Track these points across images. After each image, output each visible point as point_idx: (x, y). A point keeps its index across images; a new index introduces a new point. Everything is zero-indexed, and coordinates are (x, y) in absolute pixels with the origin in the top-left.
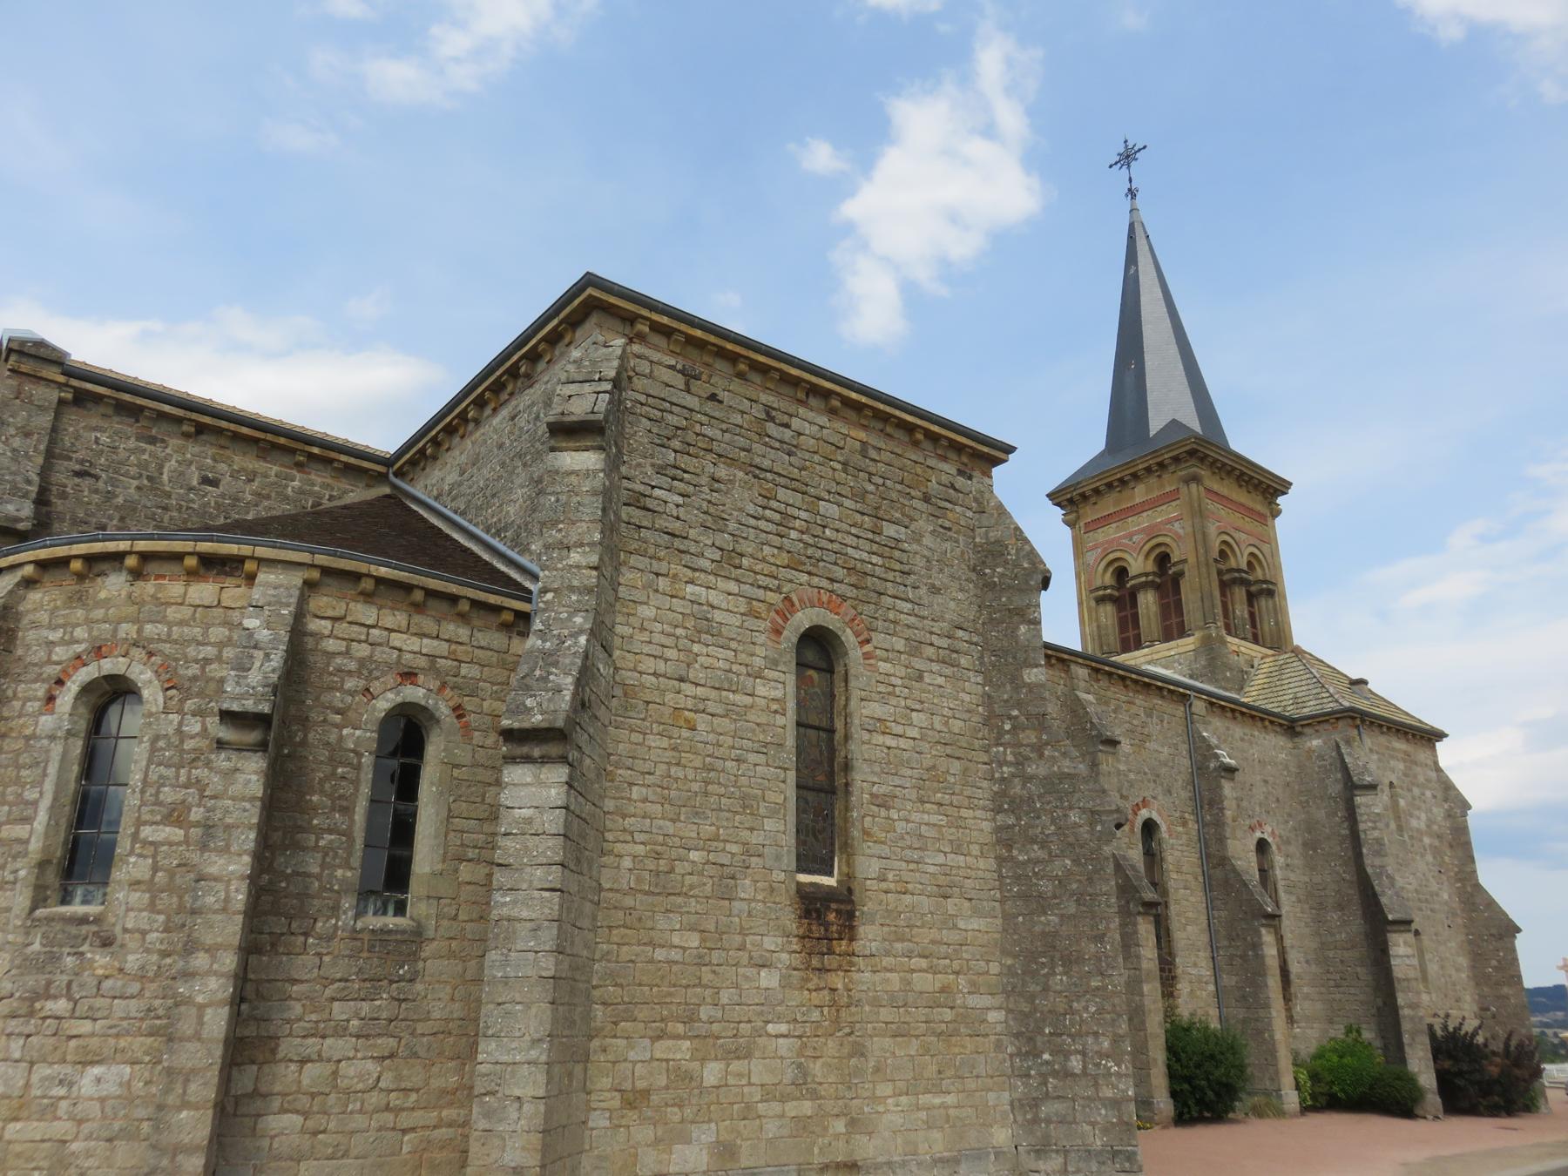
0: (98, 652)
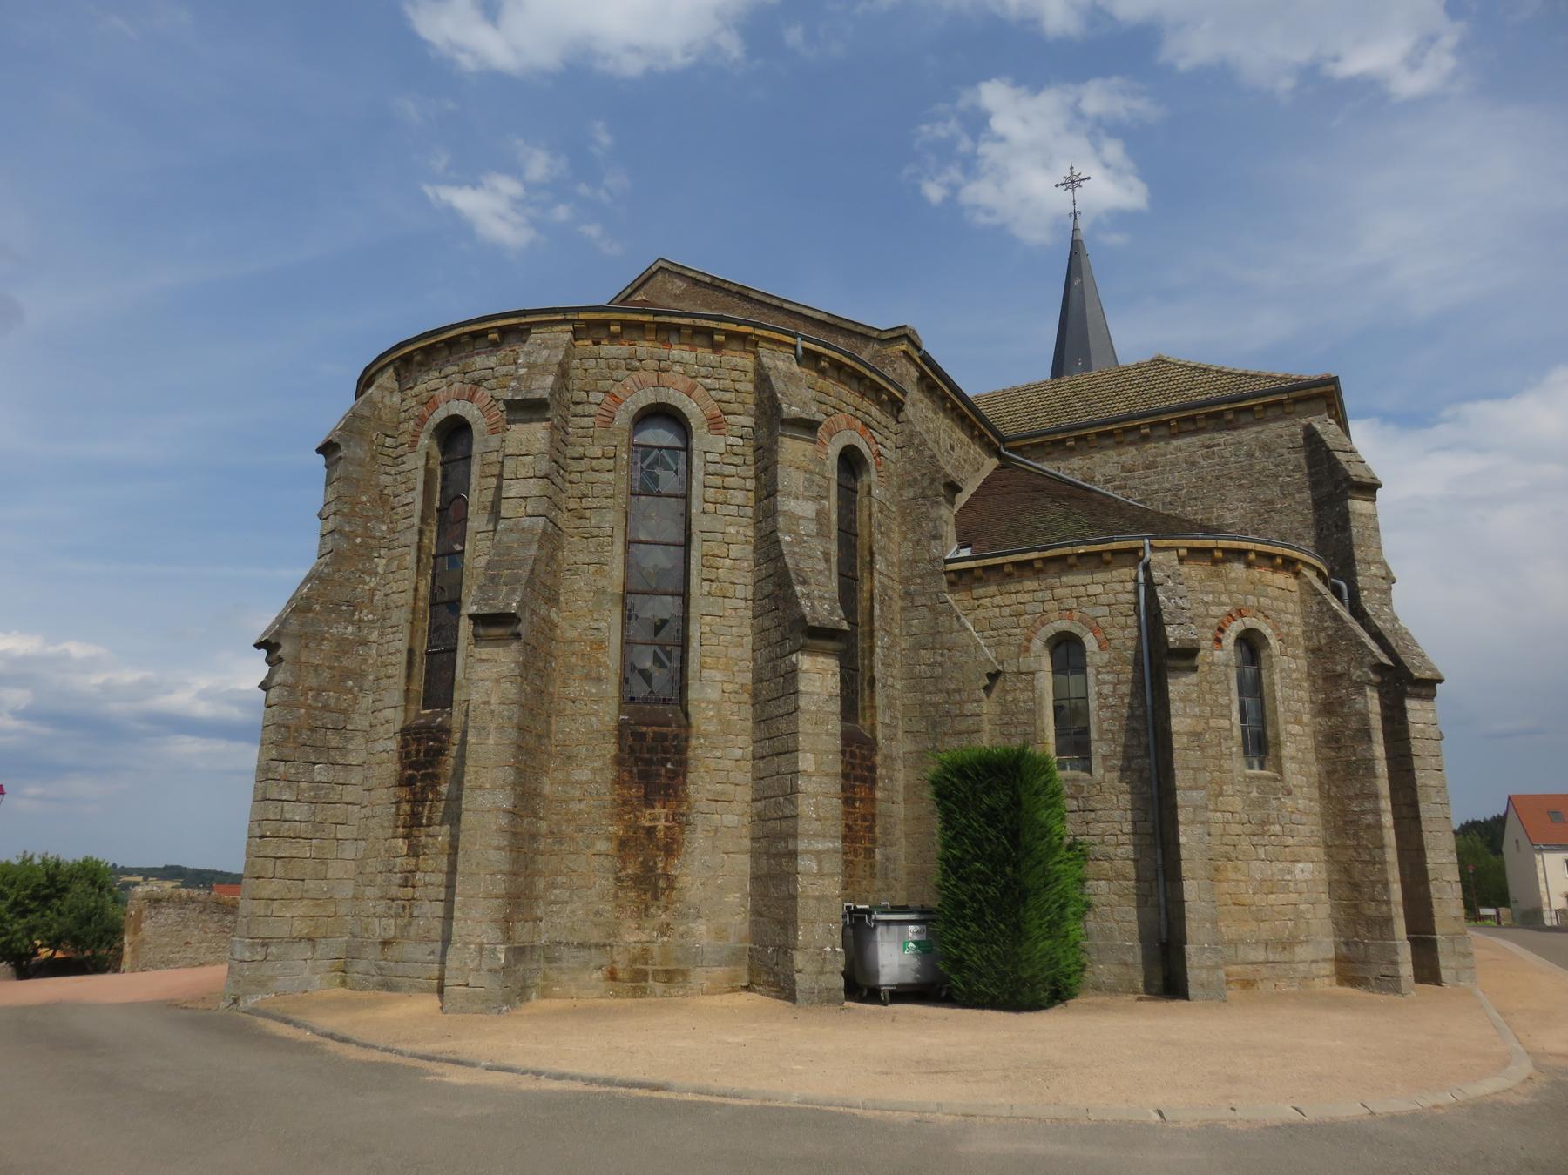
0: (422, 420)
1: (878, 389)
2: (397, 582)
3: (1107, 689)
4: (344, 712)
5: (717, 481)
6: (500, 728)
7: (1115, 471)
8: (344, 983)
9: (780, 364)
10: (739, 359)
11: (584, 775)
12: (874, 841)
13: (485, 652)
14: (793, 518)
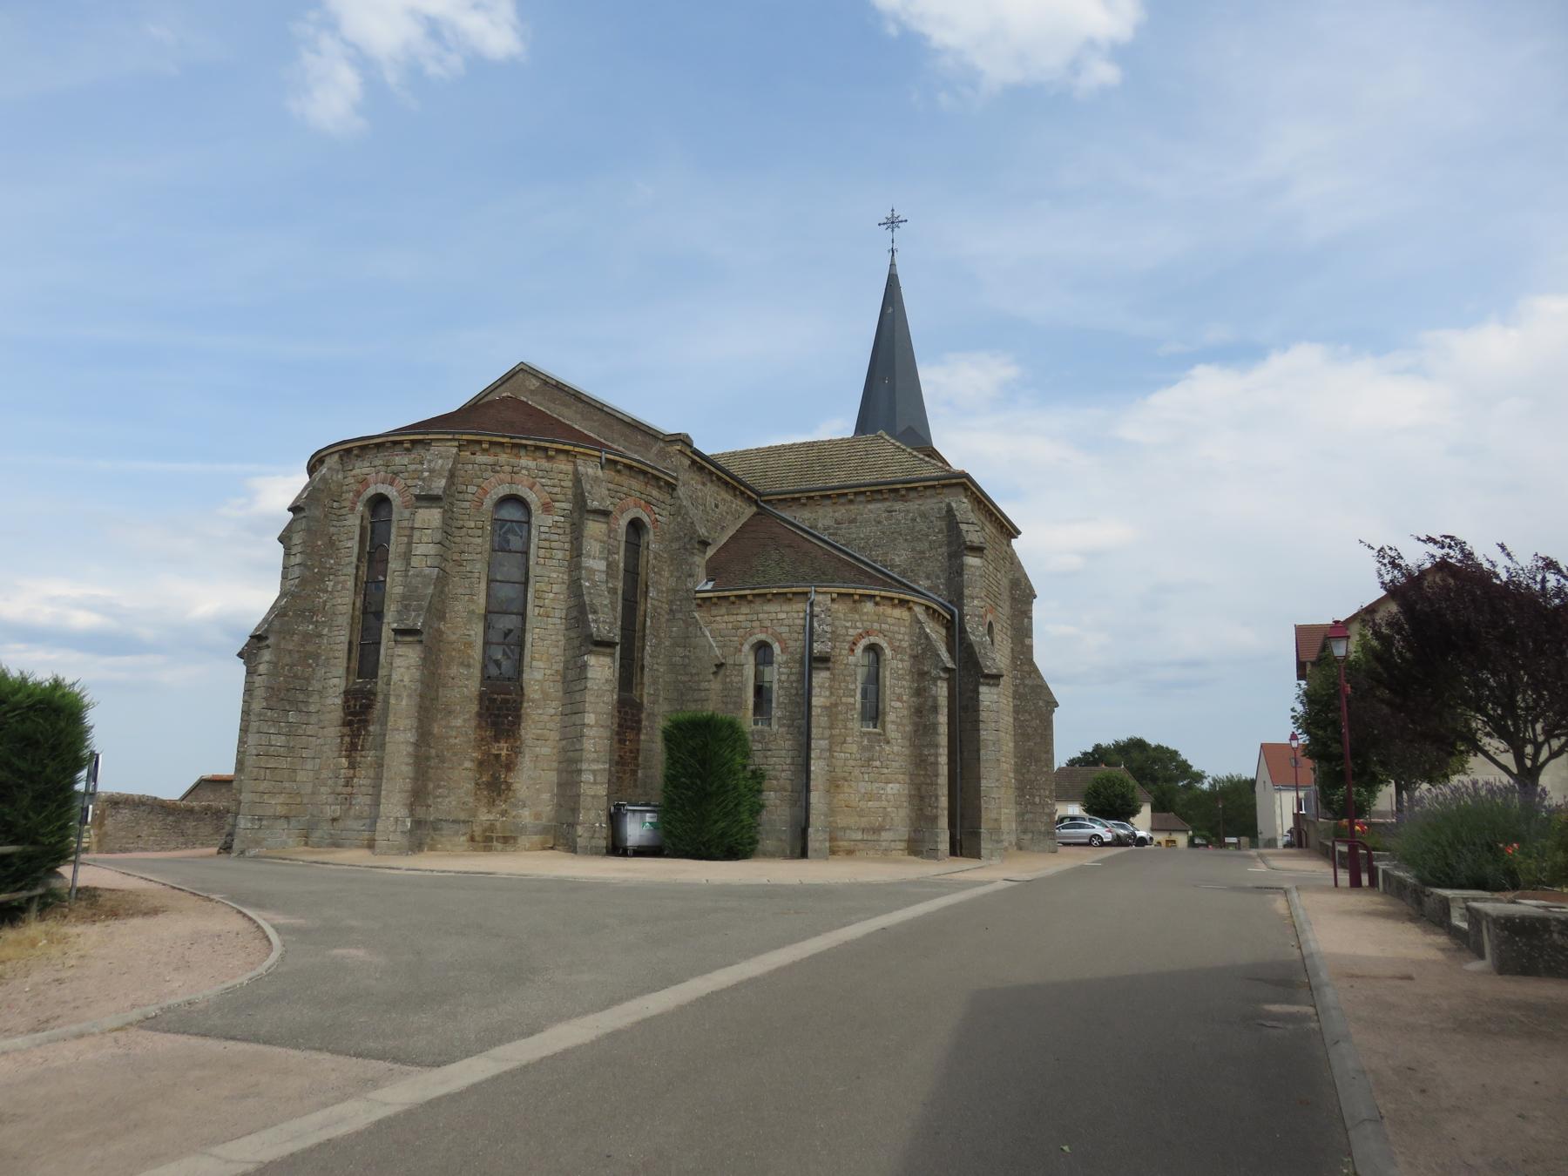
0: (358, 494)
1: (658, 478)
2: (343, 598)
3: (784, 678)
4: (307, 679)
5: (546, 544)
6: (409, 696)
7: (829, 522)
8: (306, 844)
9: (590, 471)
10: (563, 465)
11: (459, 722)
12: (637, 765)
13: (401, 650)
14: (592, 571)
